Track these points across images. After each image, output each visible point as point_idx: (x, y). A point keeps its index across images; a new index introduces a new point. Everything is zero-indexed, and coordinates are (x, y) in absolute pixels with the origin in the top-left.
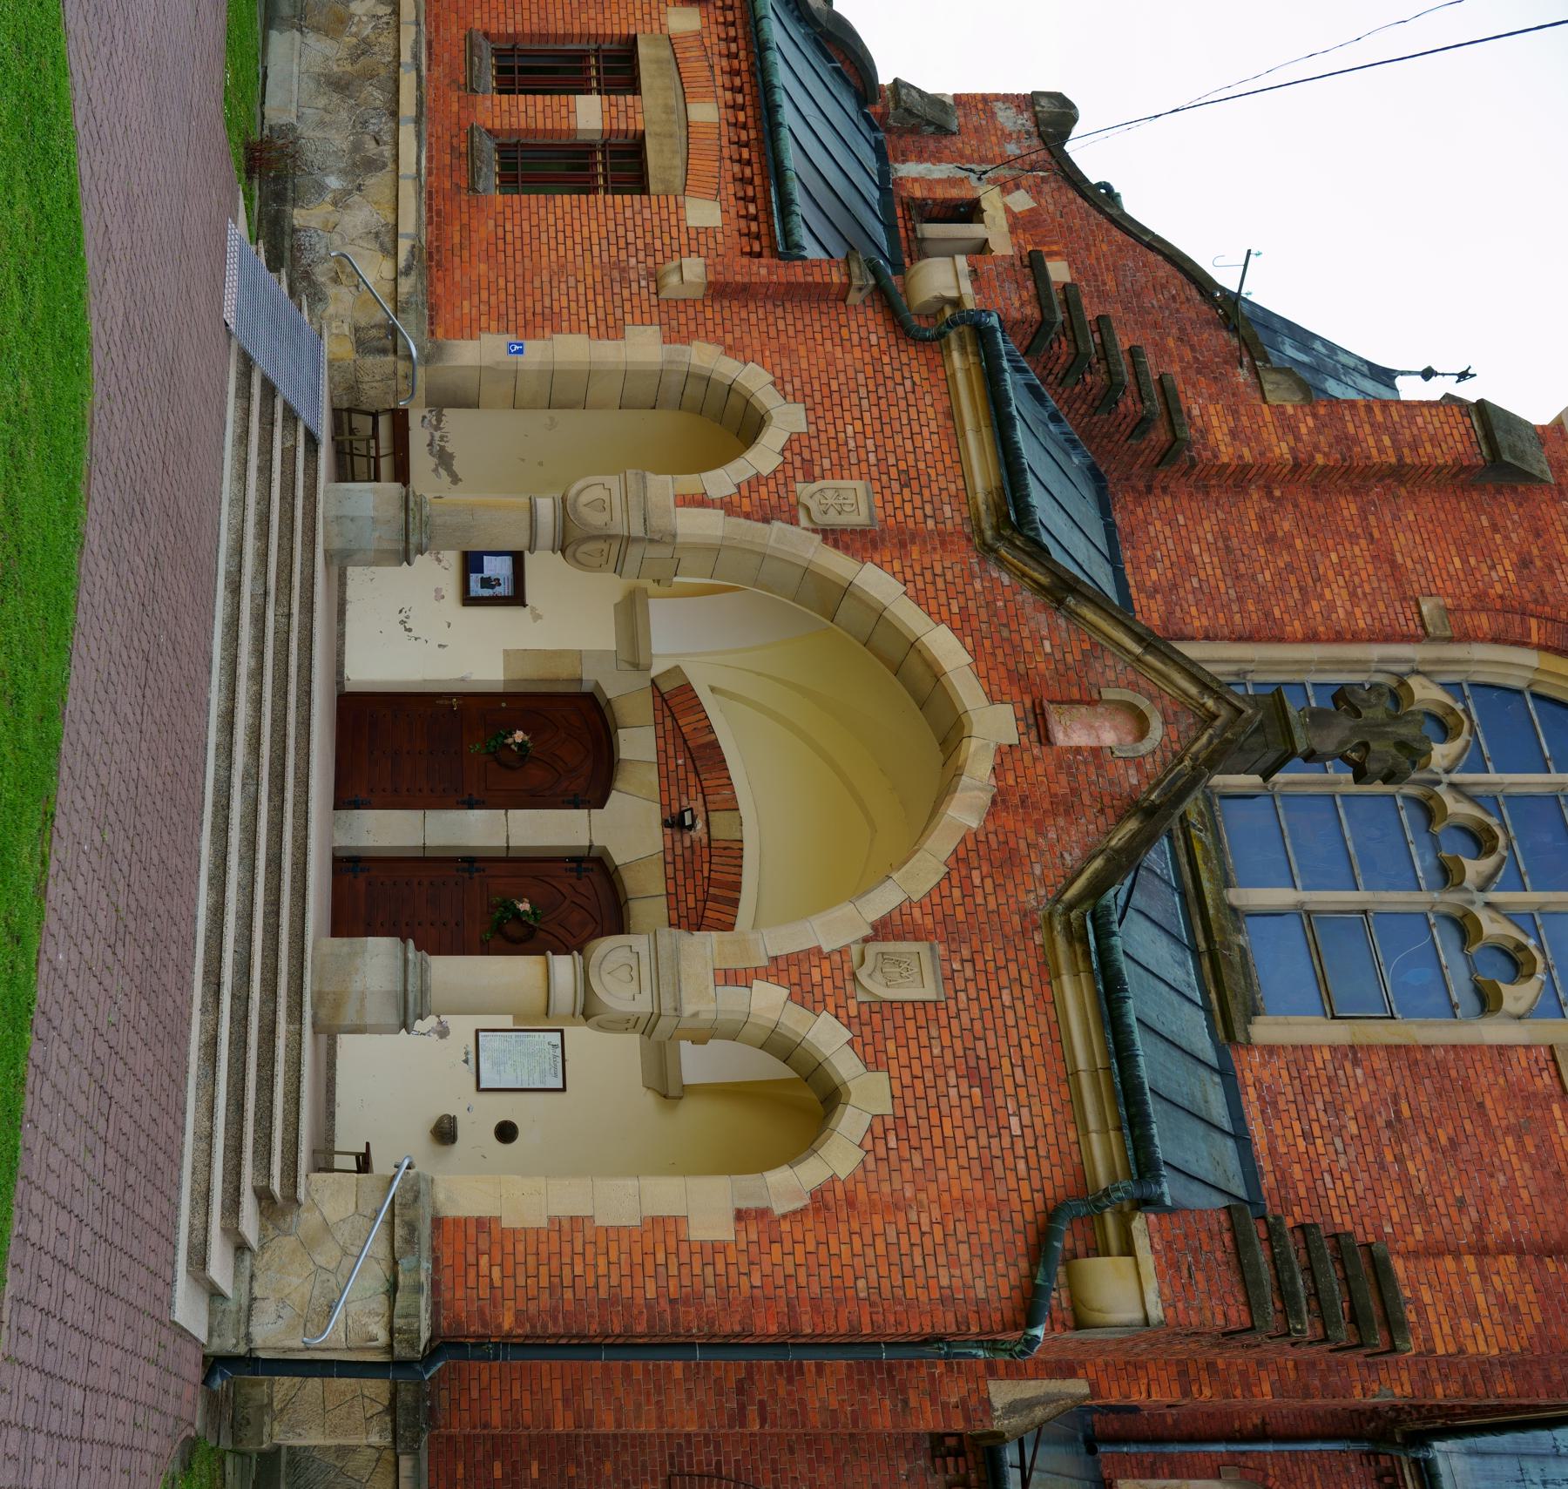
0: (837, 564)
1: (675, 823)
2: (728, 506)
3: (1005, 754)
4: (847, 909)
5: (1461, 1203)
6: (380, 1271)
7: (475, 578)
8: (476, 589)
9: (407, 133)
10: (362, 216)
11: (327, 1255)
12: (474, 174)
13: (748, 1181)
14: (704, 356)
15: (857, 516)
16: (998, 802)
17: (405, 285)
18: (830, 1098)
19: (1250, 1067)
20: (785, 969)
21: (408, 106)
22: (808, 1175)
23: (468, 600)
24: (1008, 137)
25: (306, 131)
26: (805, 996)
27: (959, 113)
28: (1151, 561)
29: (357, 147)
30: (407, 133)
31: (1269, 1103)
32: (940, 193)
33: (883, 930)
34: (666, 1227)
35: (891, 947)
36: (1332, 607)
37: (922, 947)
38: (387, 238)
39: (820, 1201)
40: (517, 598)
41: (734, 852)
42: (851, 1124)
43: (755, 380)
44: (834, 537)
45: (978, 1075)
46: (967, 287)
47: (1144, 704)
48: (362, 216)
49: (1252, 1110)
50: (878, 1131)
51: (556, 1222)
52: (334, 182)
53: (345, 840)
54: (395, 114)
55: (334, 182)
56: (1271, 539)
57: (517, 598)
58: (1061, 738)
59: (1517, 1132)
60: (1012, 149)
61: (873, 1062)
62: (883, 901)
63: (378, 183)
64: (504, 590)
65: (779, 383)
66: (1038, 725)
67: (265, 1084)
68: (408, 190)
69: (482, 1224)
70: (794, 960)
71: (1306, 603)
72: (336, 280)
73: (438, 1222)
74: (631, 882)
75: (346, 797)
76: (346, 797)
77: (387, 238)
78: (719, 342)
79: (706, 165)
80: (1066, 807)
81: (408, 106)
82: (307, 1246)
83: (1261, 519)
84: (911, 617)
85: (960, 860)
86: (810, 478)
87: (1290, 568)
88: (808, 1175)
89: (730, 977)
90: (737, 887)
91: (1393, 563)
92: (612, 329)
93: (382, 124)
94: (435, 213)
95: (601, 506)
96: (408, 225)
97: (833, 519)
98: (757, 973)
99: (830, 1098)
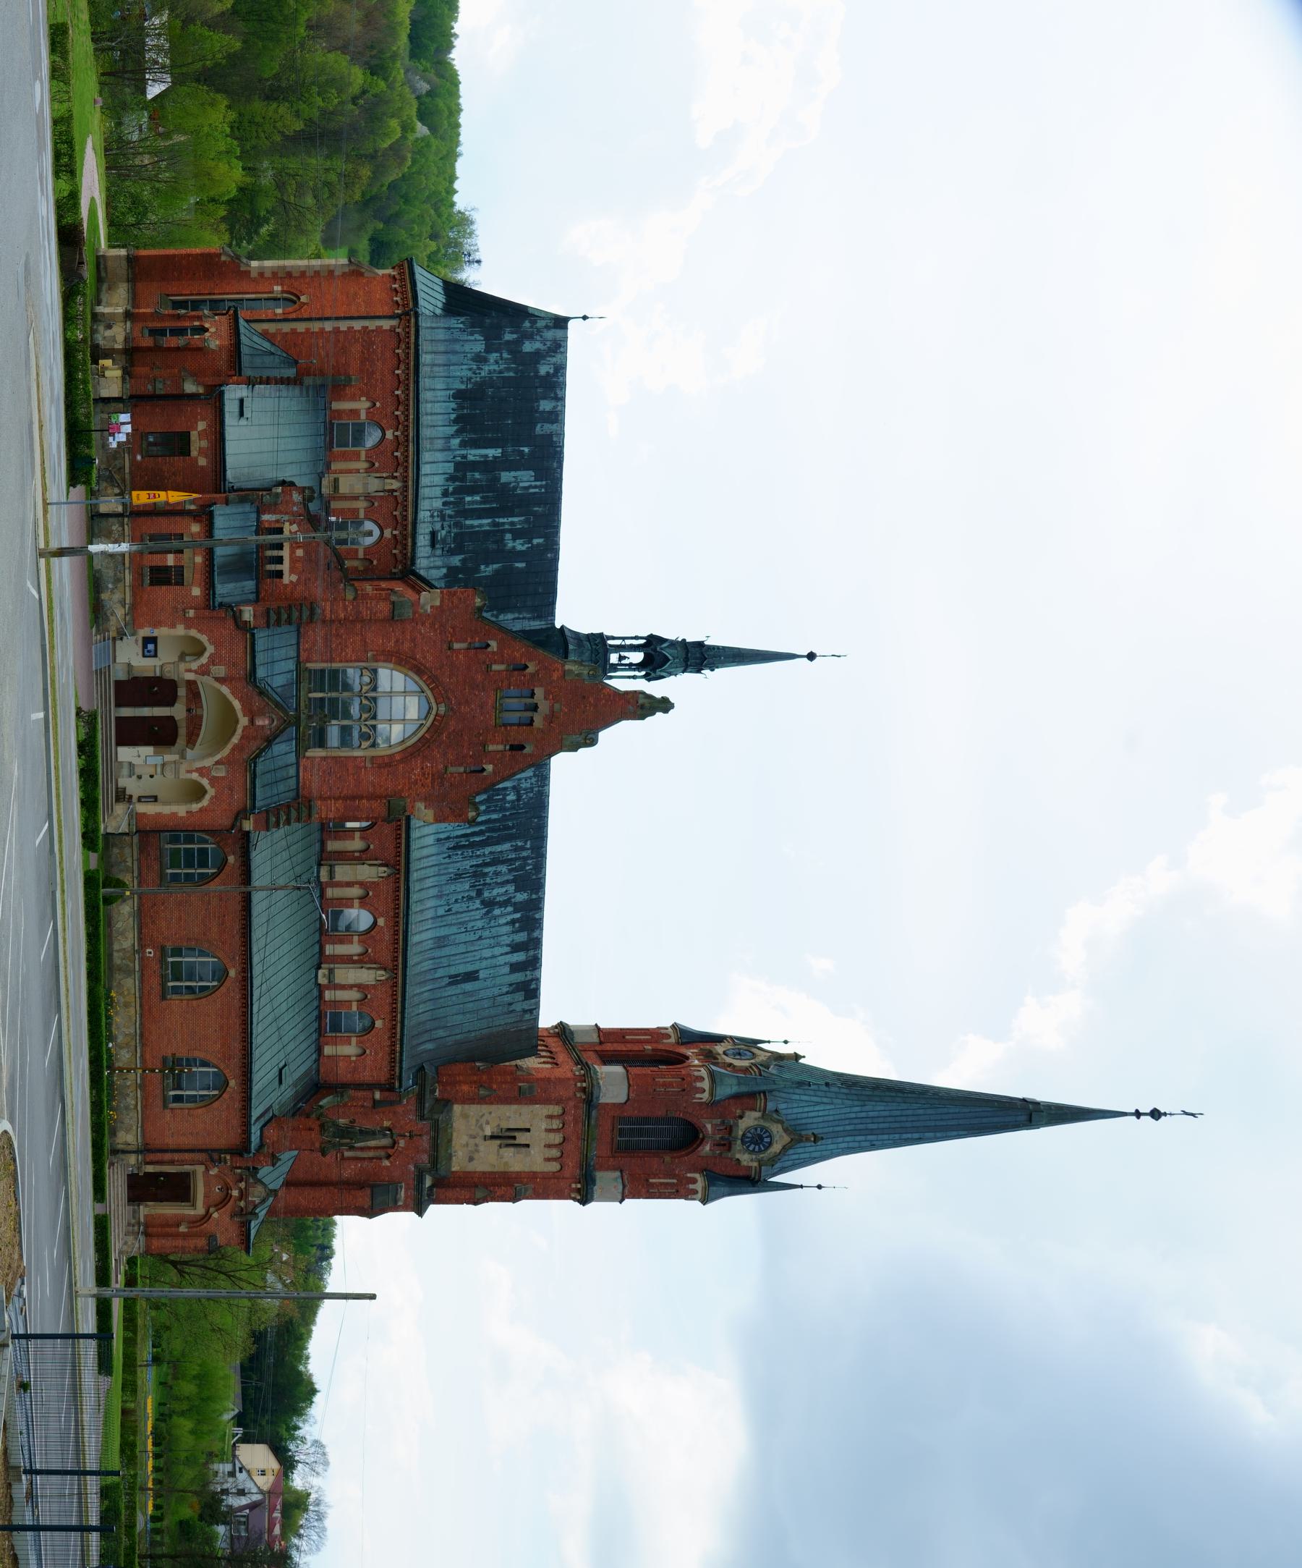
0: (217, 685)
1: (189, 710)
2: (196, 672)
3: (245, 728)
4: (211, 759)
5: (338, 788)
6: (127, 822)
7: (146, 650)
8: (146, 653)
9: (127, 571)
10: (117, 596)
11: (118, 819)
12: (143, 581)
13: (188, 806)
14: (193, 633)
15: (222, 675)
16: (242, 738)
17: (127, 618)
18: (205, 792)
19: (303, 762)
20: (198, 770)
21: (127, 565)
22: (200, 805)
23: (144, 656)
24: (294, 504)
25: (104, 570)
26: (202, 775)
27: (282, 495)
28: (307, 642)
29: (115, 575)
30: (127, 571)
31: (305, 768)
32: (273, 526)
33: (217, 763)
34: (174, 814)
35: (218, 766)
36: (347, 654)
37: (223, 766)
38: (123, 603)
39: (201, 810)
40: (155, 656)
41: (201, 718)
42: (208, 797)
43: (204, 639)
44: (217, 679)
45: (231, 789)
46: (252, 619)
47: (274, 716)
48: (117, 596)
49: (301, 770)
50: (212, 798)
51: (156, 813)
52: (110, 586)
53: (117, 715)
54: (124, 564)
55: (110, 586)
56: (338, 635)
57: (155, 656)
58: (257, 723)
59: (353, 774)
60: (295, 509)
61: (212, 787)
62: (218, 757)
63: (120, 585)
64: (152, 653)
65: (209, 640)
66: (252, 721)
67: (108, 798)
68: (127, 589)
69: (144, 814)
70: (200, 768)
71: (341, 653)
72: (112, 615)
73: (137, 813)
74: (179, 724)
75: (118, 705)
76: (118, 705)
77: (123, 603)
78: (197, 629)
79: (198, 576)
80: (255, 738)
81: (127, 565)
82: (115, 818)
83: (336, 630)
84: (231, 698)
85: (233, 749)
86: (214, 665)
87: (340, 643)
88: (200, 805)
89: (188, 772)
90: (201, 725)
91: (365, 642)
92: (173, 626)
93: (120, 567)
94: (134, 595)
95: (169, 672)
96: (128, 601)
97: (217, 676)
98: (194, 771)
99: (205, 792)
